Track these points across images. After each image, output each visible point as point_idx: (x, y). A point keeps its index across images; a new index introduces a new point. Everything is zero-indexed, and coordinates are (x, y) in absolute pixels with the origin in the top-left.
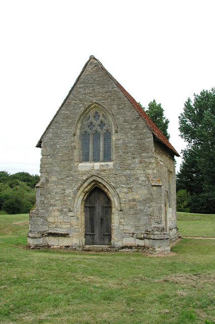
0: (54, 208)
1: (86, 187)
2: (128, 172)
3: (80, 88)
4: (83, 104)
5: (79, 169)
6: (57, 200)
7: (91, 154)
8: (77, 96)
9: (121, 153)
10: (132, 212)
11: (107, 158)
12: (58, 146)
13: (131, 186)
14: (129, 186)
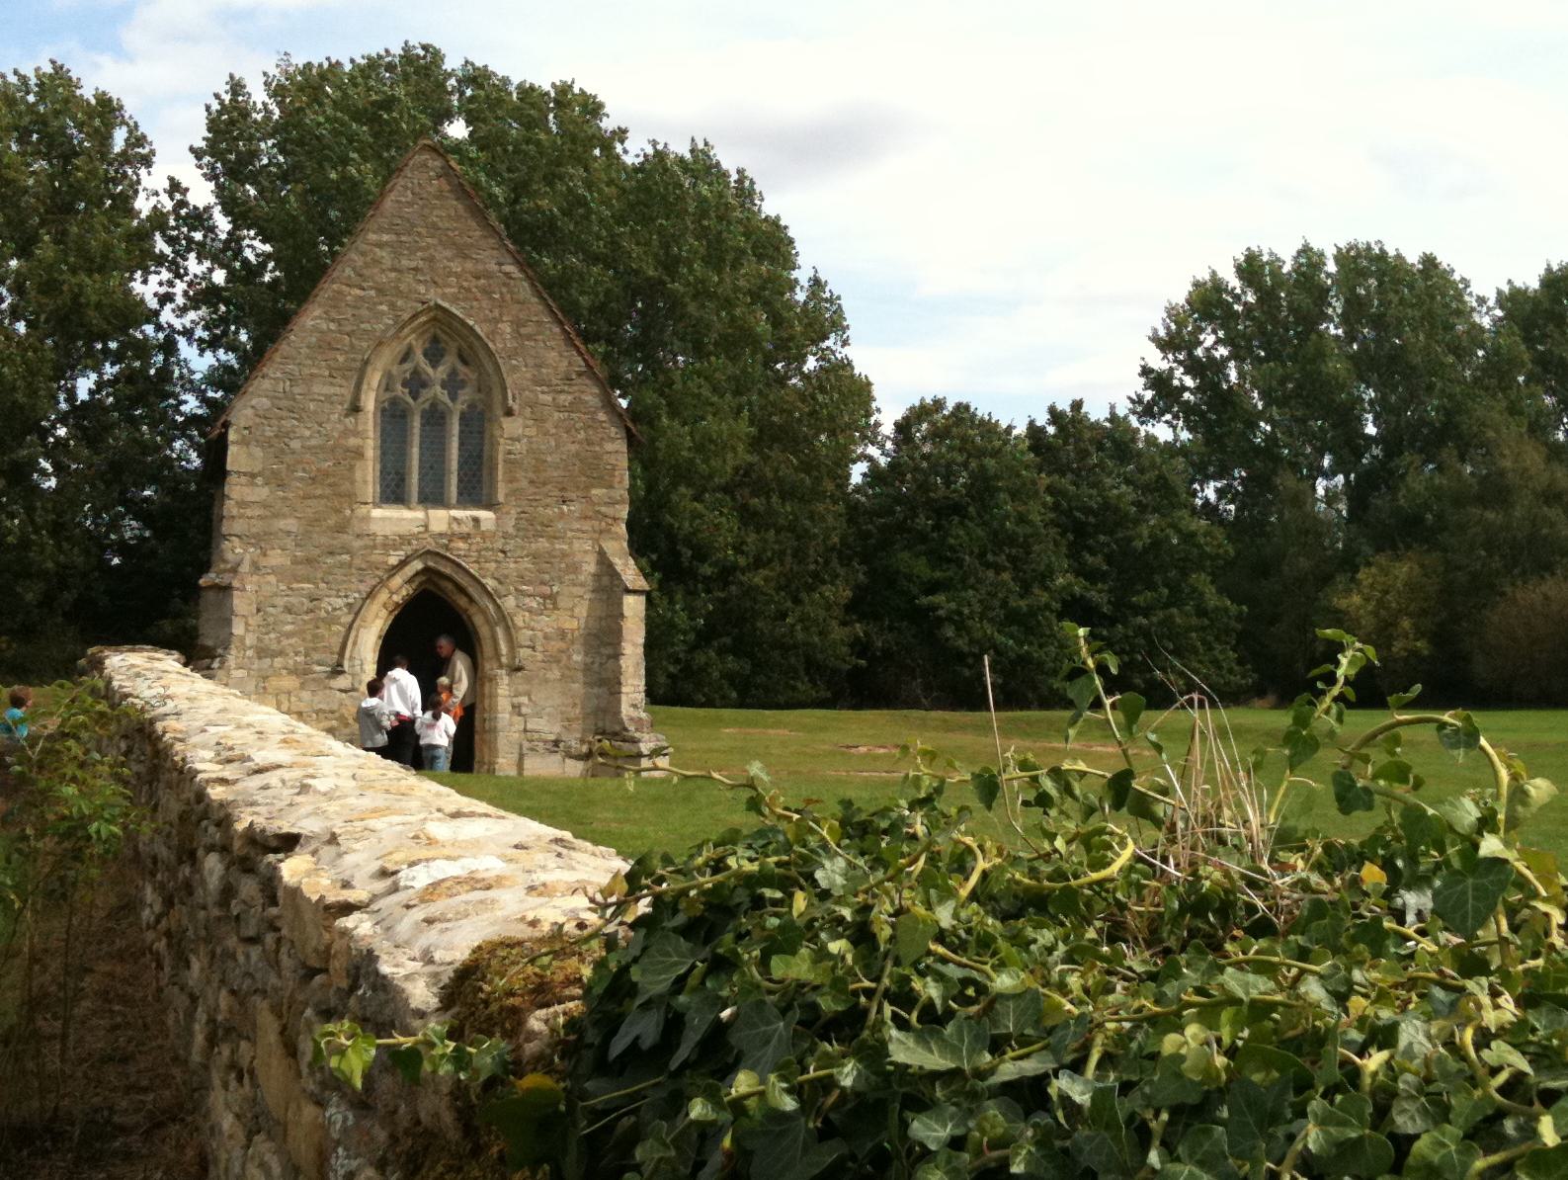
0: (278, 662)
1: (399, 589)
2: (543, 544)
3: (380, 245)
4: (392, 306)
5: (374, 528)
6: (289, 635)
7: (414, 479)
8: (366, 272)
9: (524, 484)
10: (555, 673)
11: (475, 491)
12: (295, 444)
13: (555, 589)
14: (546, 590)
